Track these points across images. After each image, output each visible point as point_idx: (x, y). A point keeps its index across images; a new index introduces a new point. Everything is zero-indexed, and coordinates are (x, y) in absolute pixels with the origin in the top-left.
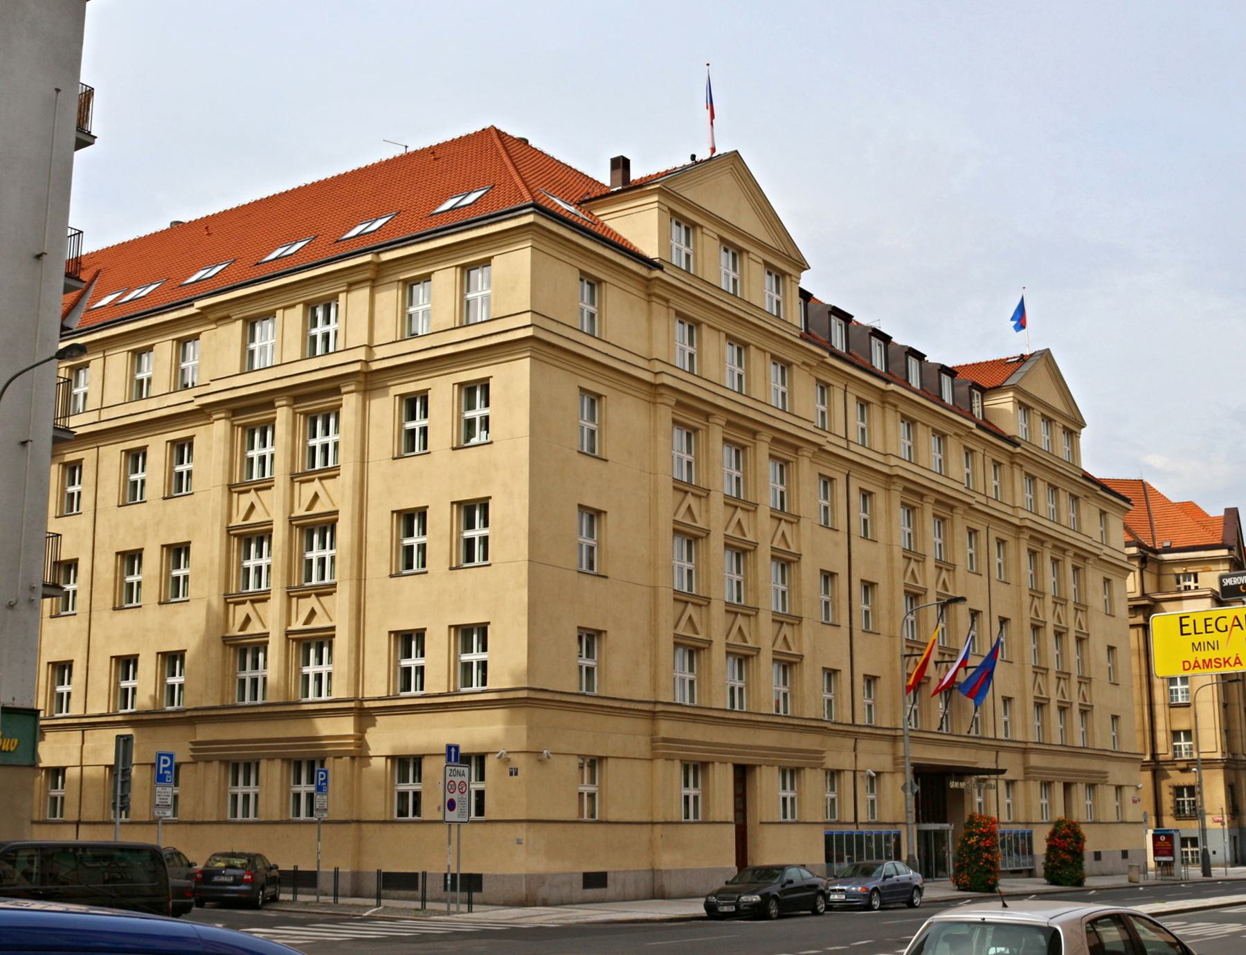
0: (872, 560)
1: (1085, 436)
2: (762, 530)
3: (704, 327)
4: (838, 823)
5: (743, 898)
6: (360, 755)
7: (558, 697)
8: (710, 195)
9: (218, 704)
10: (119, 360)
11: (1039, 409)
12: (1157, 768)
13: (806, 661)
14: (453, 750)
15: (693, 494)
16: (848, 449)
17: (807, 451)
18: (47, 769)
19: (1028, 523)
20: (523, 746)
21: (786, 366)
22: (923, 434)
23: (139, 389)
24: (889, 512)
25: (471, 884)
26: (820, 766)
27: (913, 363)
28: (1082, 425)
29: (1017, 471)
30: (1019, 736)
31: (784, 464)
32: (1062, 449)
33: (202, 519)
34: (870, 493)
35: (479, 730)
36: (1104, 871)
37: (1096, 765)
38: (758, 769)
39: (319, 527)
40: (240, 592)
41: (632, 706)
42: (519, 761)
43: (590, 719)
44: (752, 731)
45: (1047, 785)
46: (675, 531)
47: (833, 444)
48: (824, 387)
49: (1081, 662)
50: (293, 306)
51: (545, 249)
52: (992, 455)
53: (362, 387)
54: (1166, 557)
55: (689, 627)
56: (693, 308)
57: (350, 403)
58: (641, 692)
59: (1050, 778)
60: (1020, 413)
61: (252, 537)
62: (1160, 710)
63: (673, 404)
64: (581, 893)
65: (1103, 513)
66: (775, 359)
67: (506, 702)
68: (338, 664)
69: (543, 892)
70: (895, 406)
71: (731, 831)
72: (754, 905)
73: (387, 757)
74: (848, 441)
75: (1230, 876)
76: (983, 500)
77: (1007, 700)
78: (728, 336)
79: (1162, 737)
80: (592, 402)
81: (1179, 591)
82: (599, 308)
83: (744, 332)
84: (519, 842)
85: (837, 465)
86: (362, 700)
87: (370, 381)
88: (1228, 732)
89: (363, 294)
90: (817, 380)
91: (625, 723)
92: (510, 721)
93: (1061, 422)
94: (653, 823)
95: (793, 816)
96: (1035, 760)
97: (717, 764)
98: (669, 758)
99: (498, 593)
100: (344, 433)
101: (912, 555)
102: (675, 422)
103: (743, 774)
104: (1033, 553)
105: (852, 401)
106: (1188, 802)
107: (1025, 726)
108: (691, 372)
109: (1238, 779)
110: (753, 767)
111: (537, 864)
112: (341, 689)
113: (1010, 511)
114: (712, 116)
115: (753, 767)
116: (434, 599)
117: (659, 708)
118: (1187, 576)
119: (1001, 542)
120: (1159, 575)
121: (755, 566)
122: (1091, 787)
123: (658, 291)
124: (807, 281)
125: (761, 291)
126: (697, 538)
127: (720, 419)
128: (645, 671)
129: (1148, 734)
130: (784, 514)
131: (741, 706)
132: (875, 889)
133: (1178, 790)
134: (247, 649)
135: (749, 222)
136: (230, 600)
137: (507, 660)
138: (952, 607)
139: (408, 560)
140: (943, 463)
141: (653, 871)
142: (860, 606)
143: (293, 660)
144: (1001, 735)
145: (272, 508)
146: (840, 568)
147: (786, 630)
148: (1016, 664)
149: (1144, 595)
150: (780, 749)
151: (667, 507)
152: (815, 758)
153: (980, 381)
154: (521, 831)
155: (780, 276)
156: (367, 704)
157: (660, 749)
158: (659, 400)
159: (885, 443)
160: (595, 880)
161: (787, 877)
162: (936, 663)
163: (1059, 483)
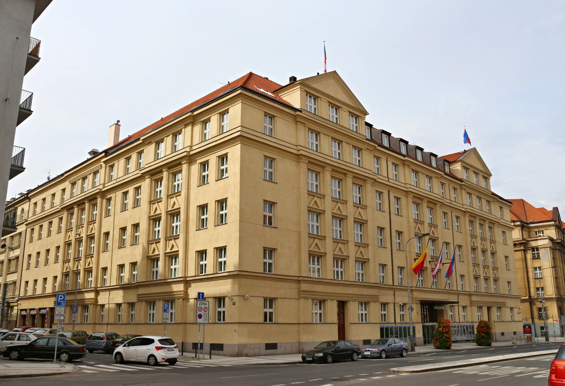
0: (399, 223)
1: (492, 179)
2: (350, 211)
3: (321, 134)
4: (388, 323)
5: (316, 355)
6: (186, 298)
7: (252, 274)
8: (325, 88)
9: (145, 280)
10: (122, 161)
11: (472, 169)
12: (531, 301)
13: (370, 261)
14: (201, 295)
15: (317, 197)
16: (388, 181)
17: (439, 205)
18: (100, 305)
19: (411, 190)
20: (237, 294)
21: (360, 150)
22: (421, 176)
23: (127, 170)
24: (407, 205)
25: (217, 348)
26: (378, 301)
27: (419, 152)
28: (490, 175)
29: (463, 191)
30: (468, 289)
31: (431, 209)
32: (483, 183)
33: (141, 215)
34: (459, 217)
35: (223, 288)
36: (506, 339)
37: (501, 300)
38: (349, 303)
39: (174, 214)
40: (153, 241)
41: (288, 278)
42: (236, 299)
43: (269, 283)
44: (345, 288)
45: (480, 308)
46: (355, 221)
47: (446, 202)
48: (443, 184)
49: (494, 262)
50: (169, 136)
51: (247, 103)
52: (452, 185)
53: (188, 161)
54: (531, 225)
55: (316, 247)
56: (316, 127)
57: (185, 167)
58: (294, 272)
59: (481, 305)
60: (464, 171)
61: (155, 220)
62: (531, 280)
63: (307, 162)
64: (264, 351)
65: (501, 208)
66: (427, 176)
67: (231, 276)
68: (178, 266)
69: (245, 351)
70: (409, 166)
71: (336, 327)
72: (321, 357)
73: (195, 299)
74: (388, 178)
75: (557, 341)
76: (449, 202)
77: (462, 276)
78: (426, 175)
79: (533, 290)
80: (380, 194)
81: (537, 237)
82: (274, 126)
83: (340, 136)
84: (235, 331)
85: (383, 187)
86: (186, 278)
87: (190, 158)
88: (558, 287)
89: (189, 128)
90: (374, 155)
91: (285, 285)
92: (233, 284)
93: (481, 174)
94: (299, 324)
95: (366, 320)
96: (474, 298)
97: (329, 301)
98: (306, 298)
99: (229, 235)
100: (181, 178)
101: (417, 221)
102: (309, 169)
103: (342, 305)
104: (471, 222)
105: (390, 164)
106: (542, 314)
107: (470, 286)
108: (359, 166)
109: (562, 305)
110: (347, 302)
111: (244, 340)
112: (179, 274)
113: (461, 206)
114: (326, 59)
115: (347, 302)
116: (206, 239)
117: (301, 279)
118: (539, 232)
119: (457, 218)
120: (529, 232)
121: (347, 225)
122: (499, 308)
123: (299, 120)
124: (368, 119)
125: (347, 122)
126: (363, 223)
127: (350, 176)
128: (295, 264)
129: (527, 289)
130: (360, 205)
131: (342, 278)
132: (383, 350)
133: (540, 309)
134: (154, 260)
135: (342, 97)
136: (149, 243)
137: (232, 260)
138: (423, 238)
139: (203, 224)
140: (481, 206)
141: (299, 342)
142: (396, 240)
143: (167, 263)
144: (459, 289)
145: (161, 209)
146: (450, 240)
147: (361, 249)
148: (466, 262)
149: (523, 239)
150: (360, 295)
151: (305, 201)
152: (375, 298)
153: (449, 160)
154: (236, 327)
155: (357, 117)
156: (188, 279)
157: (302, 295)
158: (301, 161)
159: (405, 179)
160: (271, 346)
161: (337, 346)
162: (430, 262)
163: (481, 196)
